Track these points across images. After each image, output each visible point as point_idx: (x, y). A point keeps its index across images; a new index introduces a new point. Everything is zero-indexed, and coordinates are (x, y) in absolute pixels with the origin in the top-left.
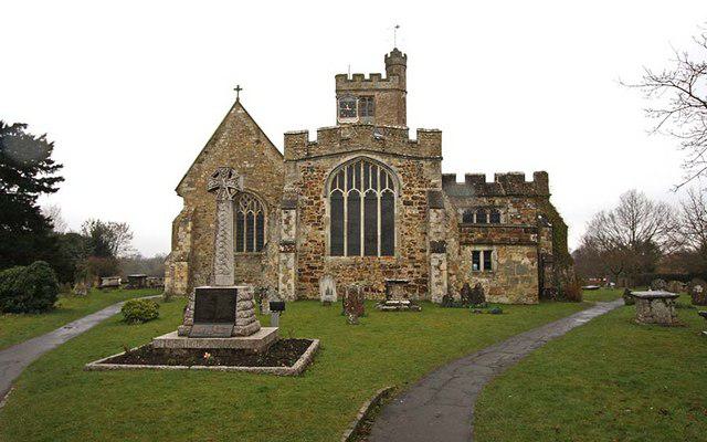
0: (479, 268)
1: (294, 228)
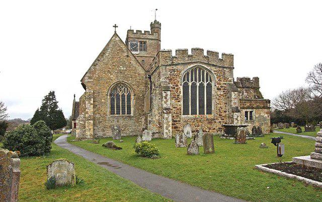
0: (247, 119)
1: (169, 101)
